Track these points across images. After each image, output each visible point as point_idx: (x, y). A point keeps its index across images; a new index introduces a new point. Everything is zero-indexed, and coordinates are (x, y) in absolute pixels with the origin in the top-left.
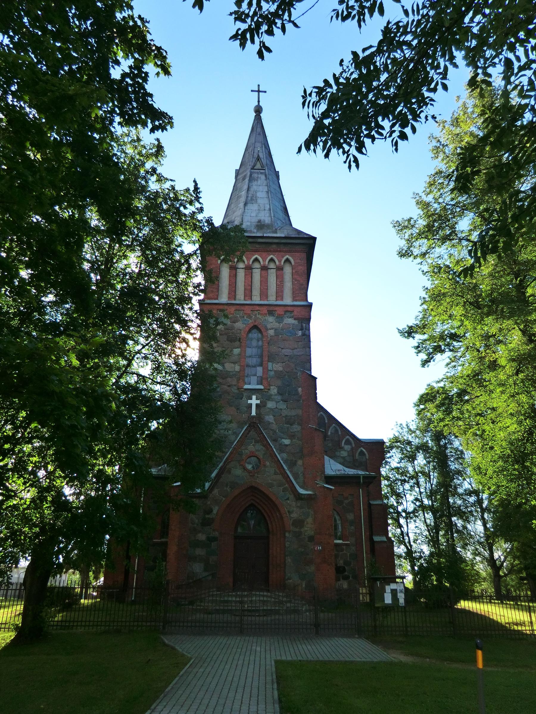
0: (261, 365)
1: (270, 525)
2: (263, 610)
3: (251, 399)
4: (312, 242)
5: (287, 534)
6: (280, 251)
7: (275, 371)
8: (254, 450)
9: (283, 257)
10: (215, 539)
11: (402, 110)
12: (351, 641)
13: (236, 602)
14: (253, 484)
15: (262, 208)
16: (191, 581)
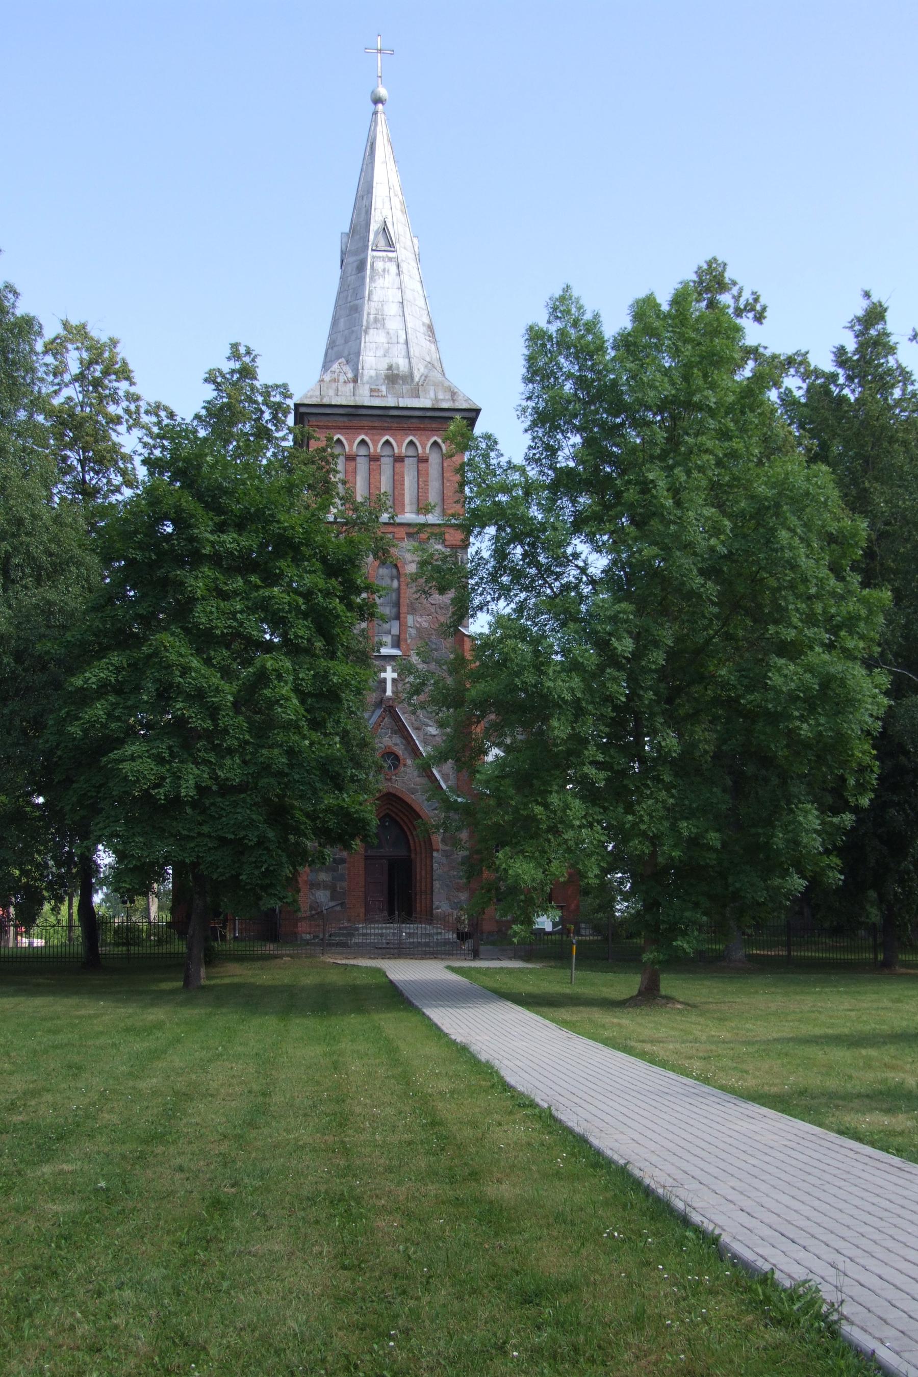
0: (398, 617)
1: (411, 842)
2: (410, 943)
3: (385, 671)
4: (473, 414)
5: (435, 854)
6: (424, 429)
7: (417, 629)
8: (390, 744)
9: (428, 440)
10: (343, 861)
11: (594, 763)
12: (446, 1013)
13: (375, 934)
14: (391, 790)
15: (394, 340)
16: (313, 912)
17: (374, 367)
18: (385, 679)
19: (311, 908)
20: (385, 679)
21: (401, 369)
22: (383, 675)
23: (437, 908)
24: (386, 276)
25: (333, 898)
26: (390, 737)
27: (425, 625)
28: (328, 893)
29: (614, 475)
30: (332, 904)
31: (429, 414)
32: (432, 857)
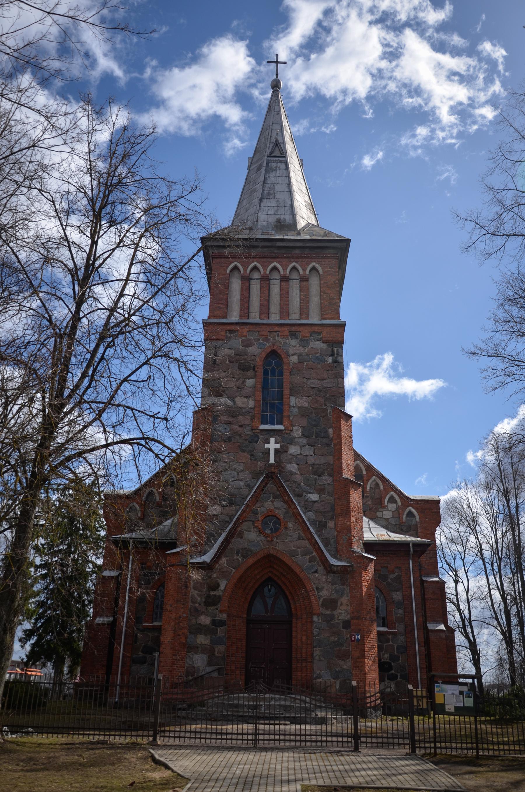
5: (315, 618)
7: (299, 408)
8: (272, 508)
14: (272, 552)
16: (190, 678)
17: (266, 220)
18: (269, 449)
19: (188, 674)
20: (269, 449)
21: (287, 221)
22: (267, 446)
23: (319, 677)
24: (278, 170)
25: (210, 664)
26: (272, 502)
27: (306, 405)
28: (205, 657)
29: (491, 133)
30: (209, 669)
31: (308, 245)
32: (312, 622)
